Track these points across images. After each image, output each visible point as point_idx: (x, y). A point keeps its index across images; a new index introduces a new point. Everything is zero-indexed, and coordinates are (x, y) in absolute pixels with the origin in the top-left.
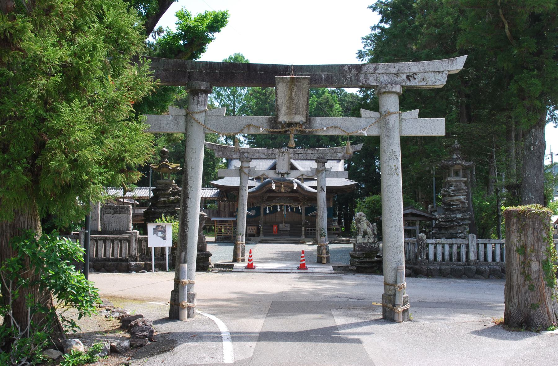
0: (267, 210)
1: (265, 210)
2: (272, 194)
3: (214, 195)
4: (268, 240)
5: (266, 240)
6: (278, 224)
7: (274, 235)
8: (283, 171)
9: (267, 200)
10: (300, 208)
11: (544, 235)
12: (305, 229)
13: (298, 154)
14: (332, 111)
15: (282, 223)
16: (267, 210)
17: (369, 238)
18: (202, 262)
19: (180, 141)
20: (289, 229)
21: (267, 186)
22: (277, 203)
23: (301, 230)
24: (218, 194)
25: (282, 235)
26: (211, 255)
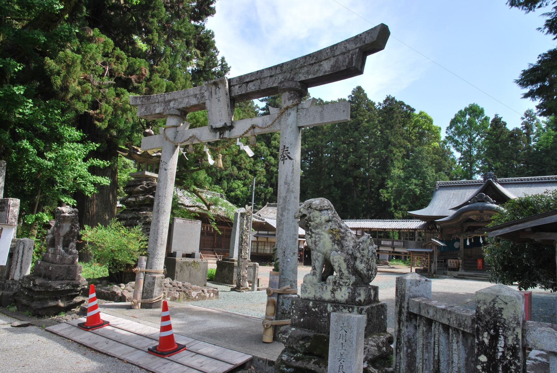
2: (472, 224)
3: (420, 226)
4: (466, 276)
5: (463, 275)
7: (478, 270)
8: (219, 125)
9: (467, 231)
13: (248, 83)
17: (337, 285)
18: (39, 300)
21: (463, 215)
24: (424, 226)
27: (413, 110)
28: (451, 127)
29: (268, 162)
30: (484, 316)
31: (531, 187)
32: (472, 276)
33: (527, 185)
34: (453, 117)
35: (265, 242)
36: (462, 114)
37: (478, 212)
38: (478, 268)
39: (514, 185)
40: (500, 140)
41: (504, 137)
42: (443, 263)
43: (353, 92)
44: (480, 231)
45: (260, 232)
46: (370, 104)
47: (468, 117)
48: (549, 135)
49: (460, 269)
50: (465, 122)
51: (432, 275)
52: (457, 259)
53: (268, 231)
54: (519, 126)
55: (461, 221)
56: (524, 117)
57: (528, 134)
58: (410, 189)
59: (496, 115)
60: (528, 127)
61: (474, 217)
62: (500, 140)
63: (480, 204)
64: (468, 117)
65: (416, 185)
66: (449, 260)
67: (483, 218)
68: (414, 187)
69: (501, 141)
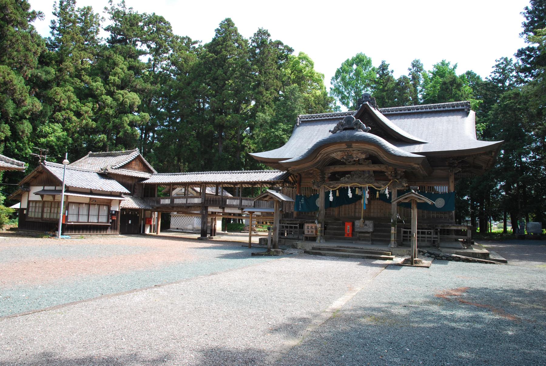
0: (331, 195)
2: (338, 169)
4: (324, 249)
6: (353, 220)
7: (345, 240)
10: (387, 192)
12: (399, 232)
15: (359, 219)
16: (331, 195)
19: (191, 165)
20: (371, 230)
21: (323, 151)
25: (359, 239)
26: (89, 9)
27: (290, 50)
28: (337, 77)
29: (104, 102)
31: (421, 117)
32: (333, 250)
33: (416, 116)
34: (339, 66)
35: (51, 202)
36: (349, 63)
37: (344, 146)
38: (346, 236)
40: (386, 88)
41: (390, 85)
43: (221, 25)
45: (47, 188)
46: (238, 39)
47: (355, 67)
48: (436, 82)
49: (318, 238)
50: (352, 71)
51: (269, 250)
52: (314, 222)
53: (56, 186)
55: (318, 162)
56: (411, 67)
57: (415, 85)
59: (383, 62)
60: (415, 78)
61: (337, 156)
62: (386, 88)
63: (347, 133)
64: (355, 67)
65: (284, 130)
66: (306, 225)
67: (351, 156)
68: (281, 132)
69: (387, 90)
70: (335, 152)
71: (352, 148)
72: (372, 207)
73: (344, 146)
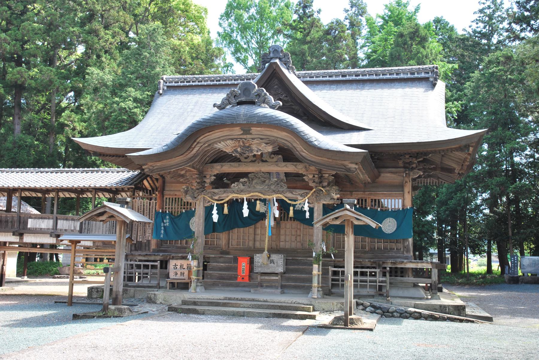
0: (215, 212)
1: (208, 211)
4: (202, 304)
11: (475, 264)
14: (424, 47)
15: (261, 251)
16: (215, 212)
21: (203, 139)
22: (241, 192)
23: (310, 272)
28: (227, 15)
30: (446, 77)
31: (362, 89)
32: (217, 304)
33: (354, 86)
38: (239, 280)
39: (328, 86)
40: (308, 38)
42: (158, 270)
44: (244, 184)
48: (389, 33)
49: (193, 285)
51: (105, 308)
54: (341, 16)
58: (121, 109)
62: (308, 38)
63: (243, 109)
65: (136, 100)
67: (249, 148)
69: (310, 42)
70: (223, 140)
71: (251, 134)
72: (282, 232)
73: (237, 131)
